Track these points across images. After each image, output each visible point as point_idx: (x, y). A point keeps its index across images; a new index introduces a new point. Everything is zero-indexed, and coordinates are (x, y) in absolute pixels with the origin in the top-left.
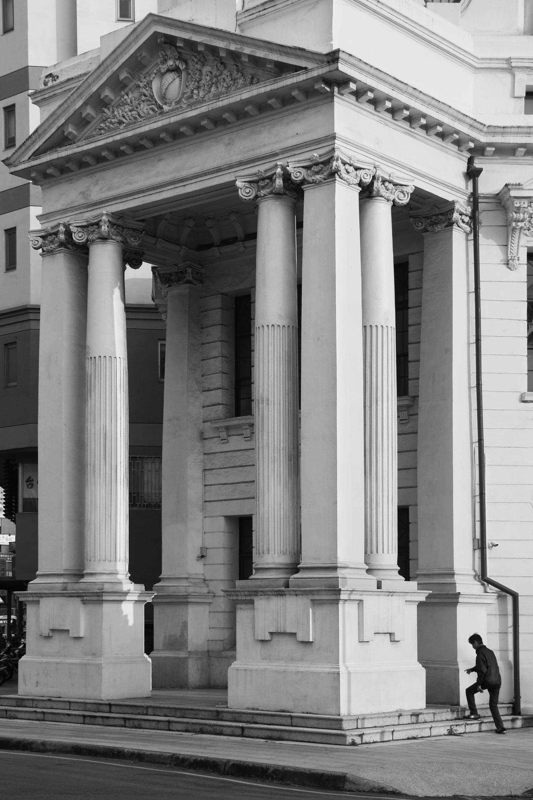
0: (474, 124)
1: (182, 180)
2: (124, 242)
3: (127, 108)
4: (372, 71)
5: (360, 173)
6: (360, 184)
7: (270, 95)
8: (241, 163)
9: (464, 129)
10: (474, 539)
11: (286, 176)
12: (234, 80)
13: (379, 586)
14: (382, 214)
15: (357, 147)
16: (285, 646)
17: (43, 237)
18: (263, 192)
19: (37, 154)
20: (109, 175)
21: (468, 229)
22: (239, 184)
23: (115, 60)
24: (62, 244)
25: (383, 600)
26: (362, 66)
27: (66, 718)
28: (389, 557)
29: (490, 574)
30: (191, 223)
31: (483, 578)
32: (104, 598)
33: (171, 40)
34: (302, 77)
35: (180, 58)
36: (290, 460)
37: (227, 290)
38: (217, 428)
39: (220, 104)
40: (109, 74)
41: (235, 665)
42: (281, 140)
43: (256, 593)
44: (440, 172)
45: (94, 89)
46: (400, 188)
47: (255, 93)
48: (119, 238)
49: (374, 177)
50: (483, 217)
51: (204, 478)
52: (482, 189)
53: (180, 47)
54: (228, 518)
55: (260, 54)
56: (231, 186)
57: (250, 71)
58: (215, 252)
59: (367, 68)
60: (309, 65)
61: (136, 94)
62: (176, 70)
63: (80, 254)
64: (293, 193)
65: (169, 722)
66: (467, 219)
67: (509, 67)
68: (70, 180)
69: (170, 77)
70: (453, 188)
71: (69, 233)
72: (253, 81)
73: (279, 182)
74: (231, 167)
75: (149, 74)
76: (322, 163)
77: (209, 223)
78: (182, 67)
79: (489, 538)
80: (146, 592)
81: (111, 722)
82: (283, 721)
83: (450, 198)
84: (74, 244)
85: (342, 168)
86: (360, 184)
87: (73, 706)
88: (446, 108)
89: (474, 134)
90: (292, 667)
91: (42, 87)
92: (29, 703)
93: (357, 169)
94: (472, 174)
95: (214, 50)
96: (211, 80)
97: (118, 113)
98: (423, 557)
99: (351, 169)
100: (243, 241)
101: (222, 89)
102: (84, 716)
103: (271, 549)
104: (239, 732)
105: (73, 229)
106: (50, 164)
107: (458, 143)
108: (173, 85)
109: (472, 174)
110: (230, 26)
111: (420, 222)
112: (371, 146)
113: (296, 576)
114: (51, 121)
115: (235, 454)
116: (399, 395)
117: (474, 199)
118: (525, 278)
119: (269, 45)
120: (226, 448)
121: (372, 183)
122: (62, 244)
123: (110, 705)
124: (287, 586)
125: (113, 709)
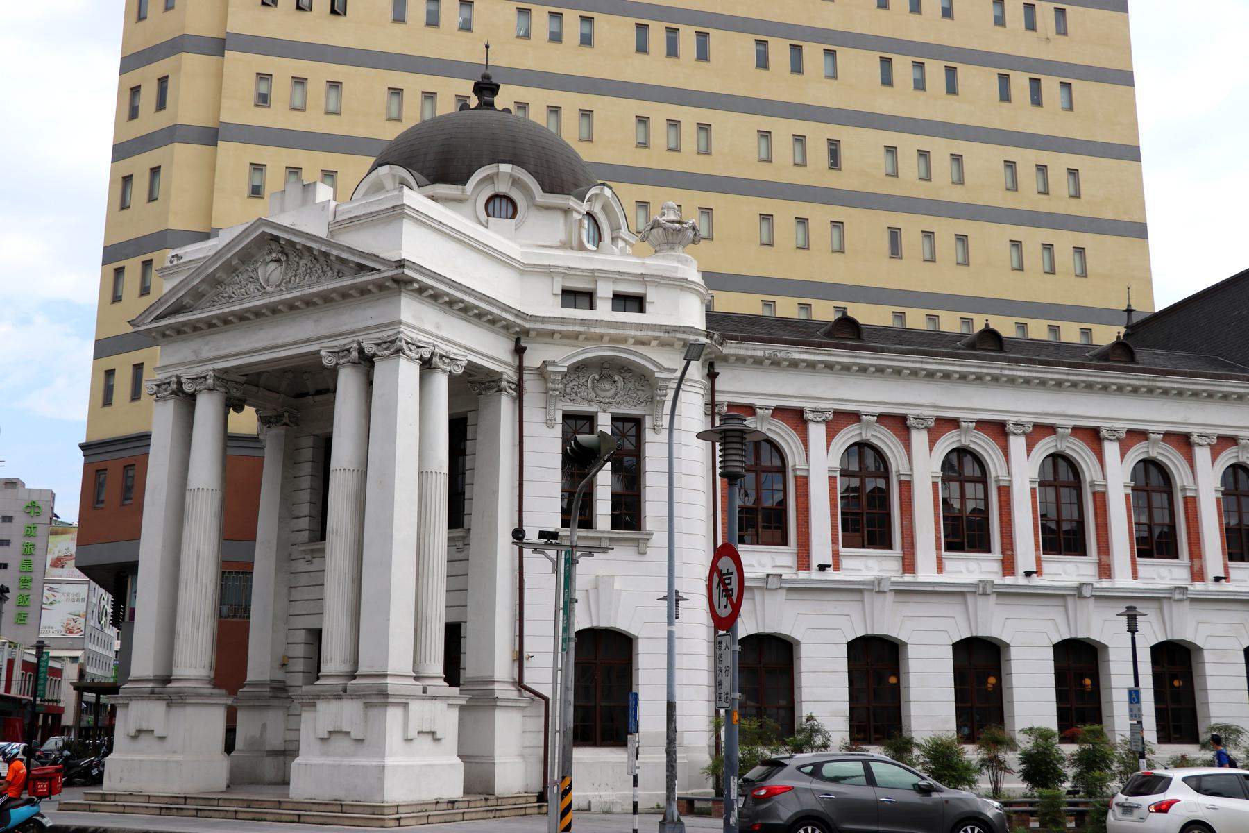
0: (519, 314)
1: (277, 347)
3: (237, 286)
5: (422, 350)
6: (421, 359)
7: (351, 287)
8: (325, 337)
9: (511, 318)
11: (361, 351)
13: (424, 691)
14: (441, 384)
15: (420, 330)
16: (340, 743)
17: (158, 386)
18: (342, 361)
19: (157, 318)
20: (217, 337)
21: (515, 394)
22: (323, 353)
23: (229, 250)
24: (173, 392)
25: (427, 704)
27: (145, 810)
28: (436, 666)
29: (526, 682)
30: (290, 375)
31: (520, 684)
32: (390, 700)
33: (276, 239)
34: (376, 276)
35: (282, 252)
36: (353, 582)
37: (317, 432)
39: (311, 291)
40: (224, 259)
41: (297, 760)
42: (357, 323)
43: (318, 697)
44: (491, 351)
45: (210, 271)
47: (339, 284)
48: (223, 390)
49: (433, 354)
50: (528, 385)
51: (290, 594)
52: (526, 363)
55: (345, 255)
57: (337, 266)
60: (382, 268)
61: (245, 276)
62: (279, 261)
63: (188, 401)
64: (366, 362)
65: (236, 812)
66: (513, 386)
67: (548, 272)
68: (185, 340)
69: (273, 266)
71: (180, 384)
72: (339, 275)
73: (355, 354)
74: (317, 339)
75: (256, 262)
77: (306, 376)
78: (283, 258)
80: (1145, 657)
81: (185, 813)
82: (334, 808)
83: (500, 369)
84: (184, 392)
85: (405, 347)
86: (421, 359)
87: (152, 800)
89: (519, 321)
90: (346, 761)
91: (169, 264)
92: (113, 798)
93: (419, 347)
94: (519, 351)
95: (310, 249)
97: (229, 290)
98: (470, 667)
101: (314, 278)
102: (161, 808)
103: (334, 661)
104: (296, 819)
105: (184, 380)
106: (169, 327)
109: (519, 351)
110: (322, 233)
111: (472, 390)
116: (450, 526)
117: (520, 369)
118: (560, 435)
119: (351, 250)
121: (431, 359)
122: (173, 392)
123: (185, 798)
124: (345, 691)
125: (188, 801)
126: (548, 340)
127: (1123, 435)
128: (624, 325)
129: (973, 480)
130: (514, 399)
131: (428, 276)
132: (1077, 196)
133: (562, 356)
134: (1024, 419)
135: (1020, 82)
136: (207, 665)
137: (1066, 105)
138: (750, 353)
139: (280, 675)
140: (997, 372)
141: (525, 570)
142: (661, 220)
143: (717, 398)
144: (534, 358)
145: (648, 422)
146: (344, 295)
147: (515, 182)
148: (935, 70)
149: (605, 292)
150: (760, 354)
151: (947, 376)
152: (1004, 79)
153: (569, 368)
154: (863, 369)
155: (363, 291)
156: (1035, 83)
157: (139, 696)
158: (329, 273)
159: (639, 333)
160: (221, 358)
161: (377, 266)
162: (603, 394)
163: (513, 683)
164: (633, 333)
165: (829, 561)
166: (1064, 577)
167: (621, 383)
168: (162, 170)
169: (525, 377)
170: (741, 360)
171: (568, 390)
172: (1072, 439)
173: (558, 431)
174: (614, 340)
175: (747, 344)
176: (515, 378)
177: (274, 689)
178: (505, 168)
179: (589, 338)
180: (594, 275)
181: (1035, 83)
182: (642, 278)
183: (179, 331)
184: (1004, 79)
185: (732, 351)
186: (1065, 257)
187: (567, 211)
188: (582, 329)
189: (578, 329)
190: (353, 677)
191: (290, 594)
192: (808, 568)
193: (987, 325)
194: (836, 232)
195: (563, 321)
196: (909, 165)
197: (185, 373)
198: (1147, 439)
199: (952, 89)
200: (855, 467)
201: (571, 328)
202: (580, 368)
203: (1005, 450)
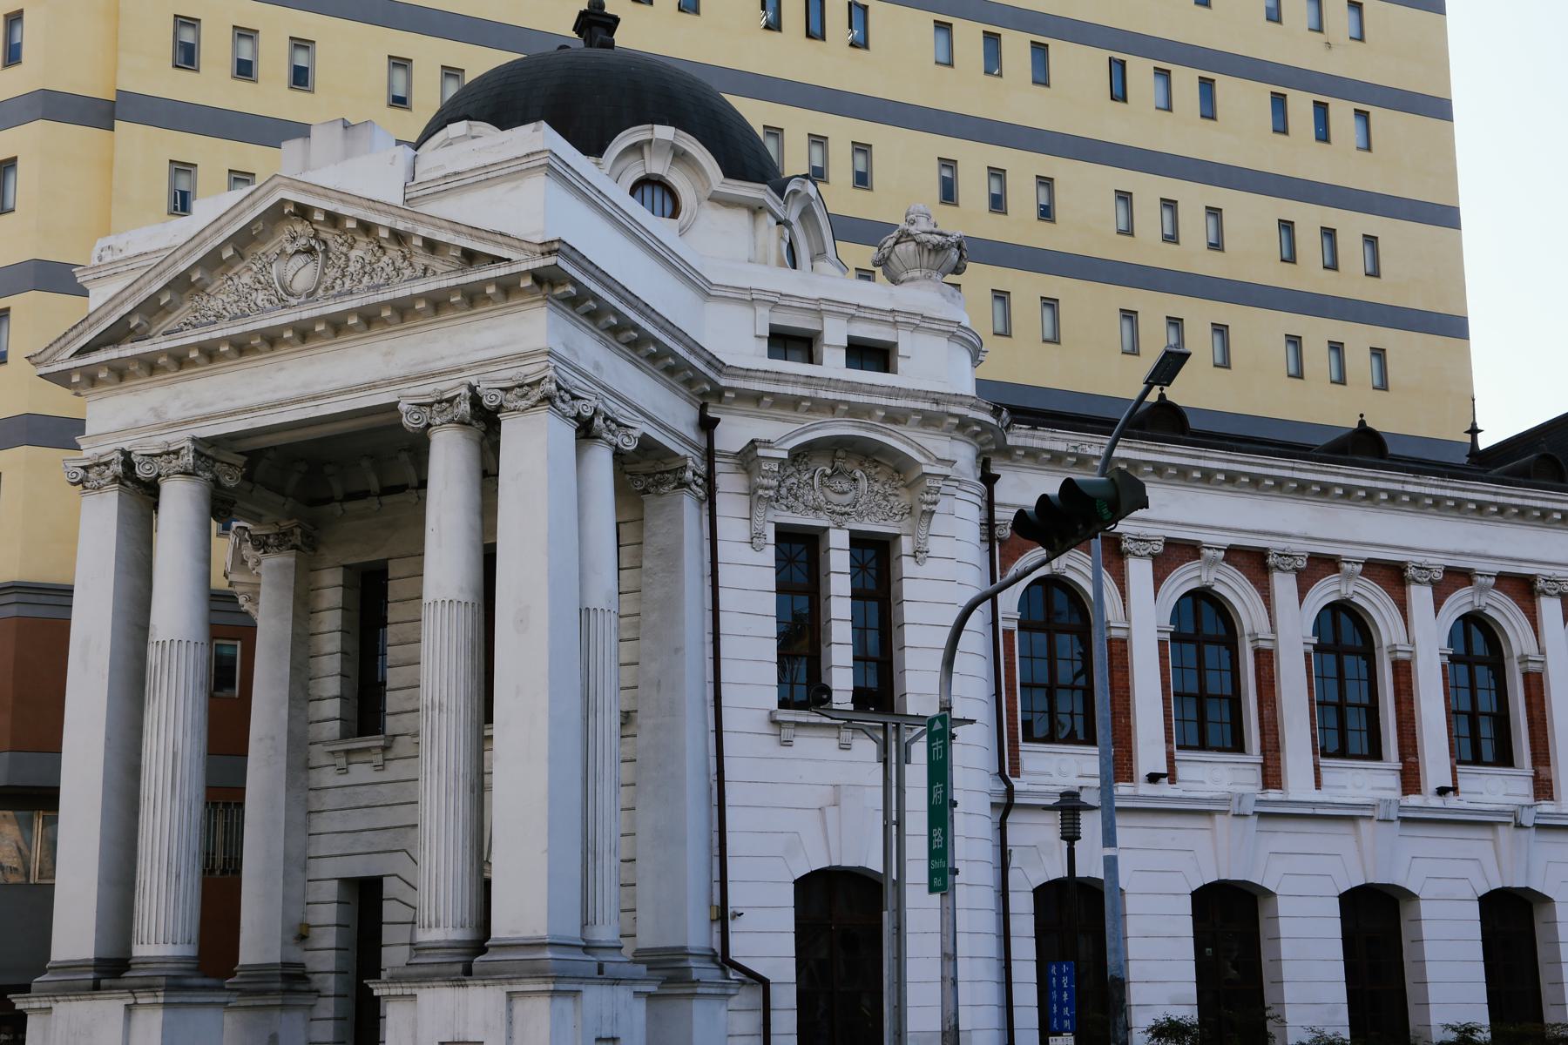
2: (216, 483)
4: (597, 273)
5: (579, 404)
10: (711, 906)
11: (476, 400)
12: (398, 270)
13: (600, 972)
19: (82, 352)
22: (403, 407)
26: (585, 264)
29: (735, 953)
31: (724, 960)
33: (303, 212)
35: (315, 237)
36: (472, 791)
38: (333, 752)
44: (662, 411)
45: (182, 267)
46: (623, 430)
48: (208, 475)
53: (318, 222)
54: (345, 882)
56: (392, 407)
57: (421, 260)
58: (336, 508)
59: (592, 269)
62: (310, 251)
64: (485, 422)
67: (749, 299)
69: (300, 260)
70: (685, 440)
73: (465, 408)
76: (529, 385)
79: (732, 902)
83: (682, 452)
84: (137, 481)
88: (681, 336)
91: (96, 262)
93: (575, 397)
94: (707, 425)
96: (363, 267)
99: (567, 397)
100: (379, 495)
105: (136, 460)
107: (689, 383)
108: (303, 274)
112: (590, 370)
113: (481, 958)
114: (110, 306)
115: (358, 789)
120: (343, 780)
121: (592, 419)
122: (116, 479)
126: (751, 408)
127: (1302, 564)
128: (871, 389)
129: (1353, 652)
130: (701, 501)
131: (592, 276)
132: (1375, 273)
133: (779, 433)
134: (1431, 561)
135: (1300, 104)
136: (195, 938)
137: (1363, 144)
138: (1047, 445)
139: (296, 955)
140: (1398, 487)
141: (727, 777)
142: (913, 229)
143: (997, 515)
144: (734, 432)
145: (906, 545)
146: (438, 303)
147: (680, 156)
148: (1186, 80)
149: (835, 334)
150: (1060, 446)
151: (1325, 490)
152: (1279, 102)
153: (790, 451)
154: (1207, 476)
155: (473, 297)
156: (1321, 110)
157: (70, 991)
158: (408, 273)
159: (893, 403)
160: (207, 418)
161: (505, 253)
162: (835, 498)
163: (713, 957)
164: (883, 401)
165: (1162, 768)
166: (1486, 797)
167: (863, 484)
168: (19, 163)
169: (718, 467)
170: (1032, 454)
171: (784, 491)
172: (1231, 570)
173: (769, 555)
174: (855, 411)
175: (1043, 432)
176: (703, 469)
177: (287, 978)
178: (664, 132)
179: (832, 407)
180: (819, 309)
181: (1321, 110)
182: (893, 317)
183: (120, 372)
184: (1279, 102)
185: (1021, 442)
186: (1359, 364)
187: (756, 210)
188: (806, 392)
189: (800, 391)
190: (482, 950)
191: (308, 824)
192: (1129, 777)
193: (1362, 423)
194: (1048, 312)
195: (779, 377)
196: (1149, 219)
197: (140, 445)
198: (1337, 570)
199: (1209, 112)
200: (1189, 629)
201: (789, 390)
202: (801, 455)
203: (1403, 606)
